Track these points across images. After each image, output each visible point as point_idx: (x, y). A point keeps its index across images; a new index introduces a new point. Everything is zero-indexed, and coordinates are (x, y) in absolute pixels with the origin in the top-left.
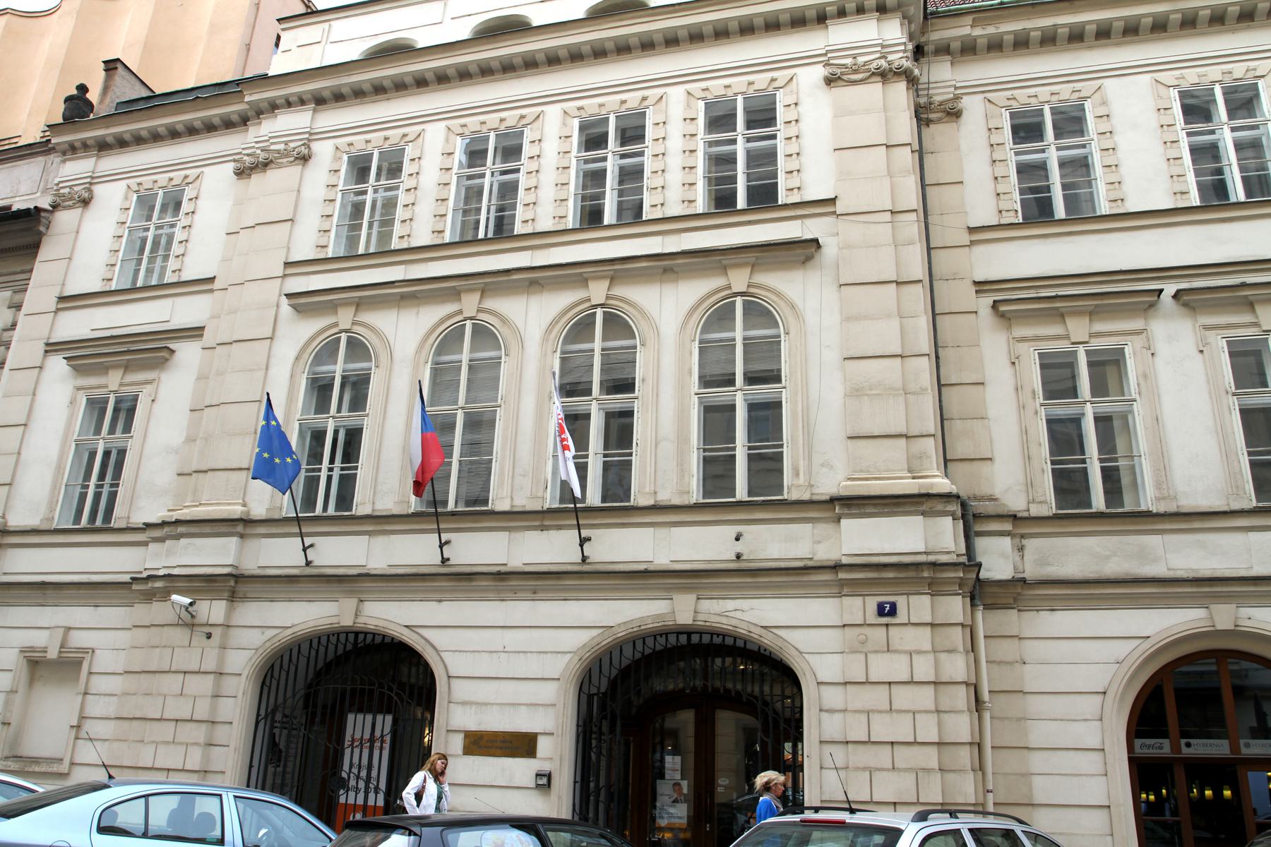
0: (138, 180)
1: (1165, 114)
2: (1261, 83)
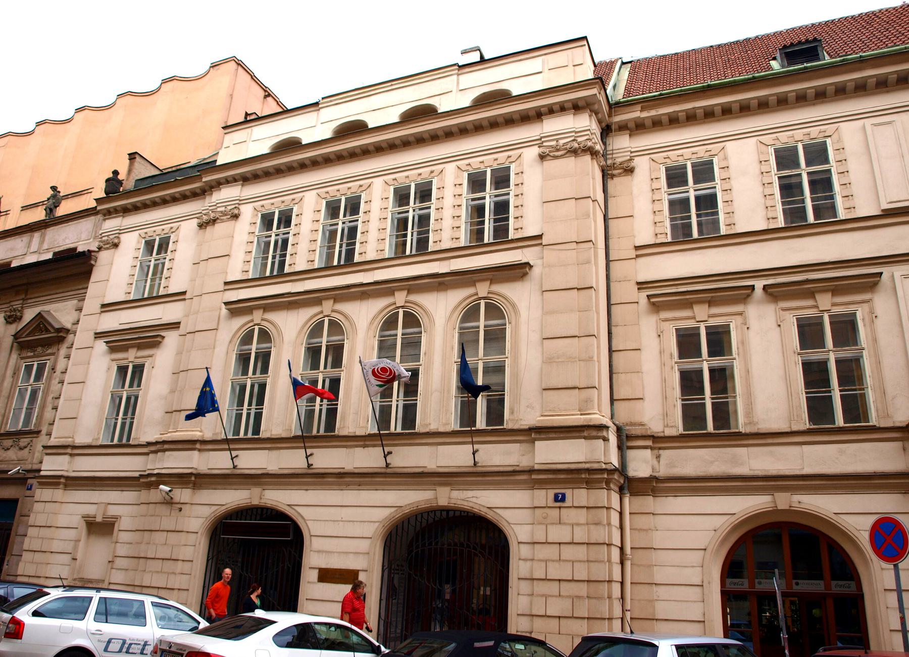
1: (765, 165)
2: (829, 141)
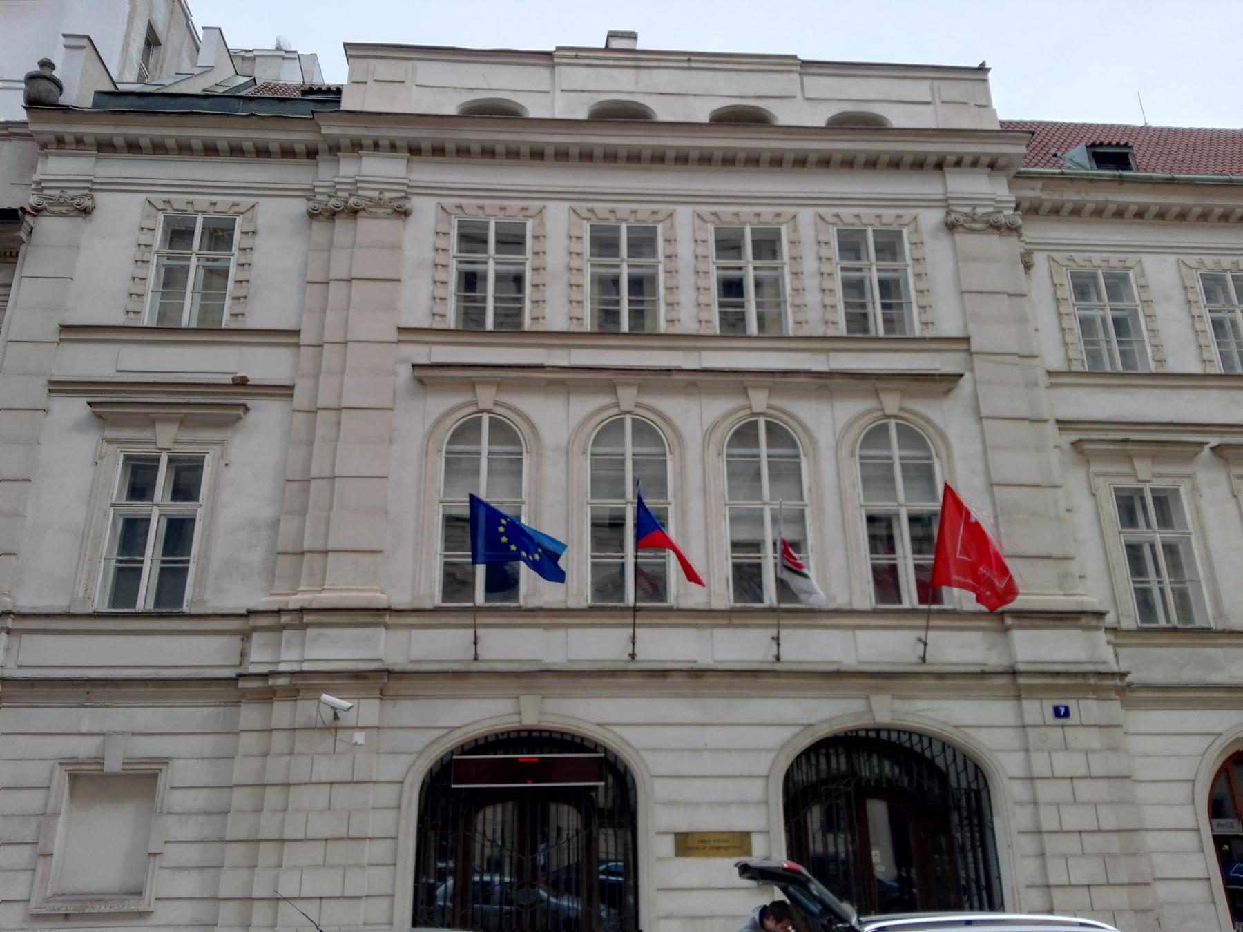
0: (166, 197)
